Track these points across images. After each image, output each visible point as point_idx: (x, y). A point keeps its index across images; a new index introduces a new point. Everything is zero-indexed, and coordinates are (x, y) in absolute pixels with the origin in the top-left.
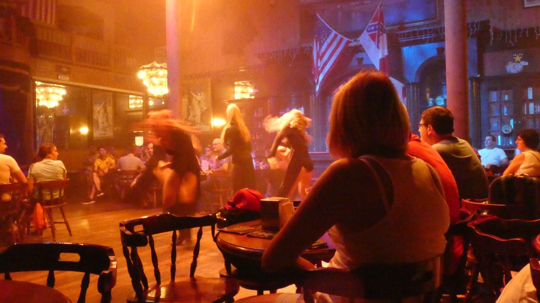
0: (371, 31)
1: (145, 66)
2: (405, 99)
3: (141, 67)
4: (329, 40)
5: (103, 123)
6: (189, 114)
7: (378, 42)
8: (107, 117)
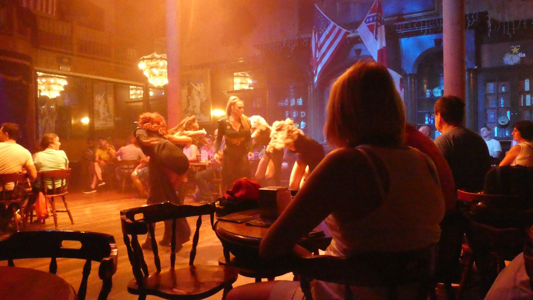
0: (369, 22)
1: (145, 57)
2: (403, 90)
3: (142, 58)
4: (327, 32)
5: (104, 114)
6: (189, 105)
7: (377, 33)
8: (108, 108)
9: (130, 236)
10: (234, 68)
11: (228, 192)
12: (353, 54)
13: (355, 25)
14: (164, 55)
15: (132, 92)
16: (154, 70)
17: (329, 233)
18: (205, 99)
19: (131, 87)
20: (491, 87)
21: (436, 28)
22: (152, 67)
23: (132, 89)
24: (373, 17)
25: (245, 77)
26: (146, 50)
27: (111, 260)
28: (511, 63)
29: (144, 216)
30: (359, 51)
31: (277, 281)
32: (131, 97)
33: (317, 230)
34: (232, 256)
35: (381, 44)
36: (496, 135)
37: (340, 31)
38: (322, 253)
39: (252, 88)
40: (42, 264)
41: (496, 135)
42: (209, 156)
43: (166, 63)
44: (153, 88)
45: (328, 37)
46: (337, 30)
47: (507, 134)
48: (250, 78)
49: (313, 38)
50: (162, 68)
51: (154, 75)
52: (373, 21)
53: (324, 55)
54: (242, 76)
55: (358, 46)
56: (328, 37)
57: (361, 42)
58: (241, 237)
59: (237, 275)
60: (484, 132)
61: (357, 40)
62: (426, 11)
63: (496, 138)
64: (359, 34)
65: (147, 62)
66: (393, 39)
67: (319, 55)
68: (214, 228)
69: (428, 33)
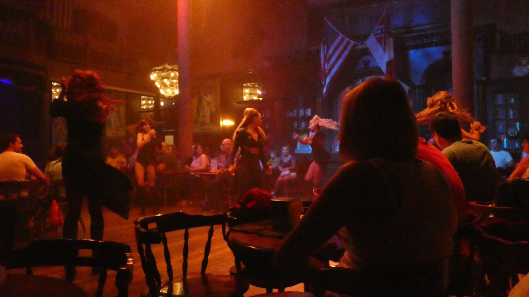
0: (378, 34)
1: (157, 68)
3: (153, 69)
4: (336, 43)
6: (199, 115)
7: (385, 45)
9: (144, 247)
10: (241, 81)
11: (239, 203)
12: (361, 65)
13: (365, 37)
14: (176, 66)
15: (143, 102)
16: (165, 81)
17: (340, 244)
18: (214, 109)
19: (143, 97)
20: (500, 99)
21: (445, 40)
22: (163, 78)
23: (144, 99)
24: (381, 29)
25: (255, 88)
26: (158, 61)
27: (128, 270)
28: (519, 74)
29: (157, 225)
30: (367, 63)
31: (289, 292)
32: (142, 107)
33: (330, 242)
34: (243, 266)
35: (389, 56)
36: (505, 146)
37: (348, 43)
38: (333, 264)
39: (261, 99)
40: (57, 272)
41: (505, 146)
42: (218, 166)
43: (177, 74)
44: (164, 97)
45: (336, 48)
46: (345, 42)
47: (517, 146)
48: (259, 89)
49: (322, 50)
50: (173, 79)
51: (165, 86)
52: (381, 33)
53: (333, 66)
54: (252, 87)
55: (367, 58)
56: (336, 48)
57: (370, 54)
58: (253, 248)
59: (248, 285)
60: (494, 144)
61: (366, 52)
62: (432, 24)
63: (505, 150)
64: (368, 46)
65: (158, 73)
66: (401, 52)
67: (327, 67)
68: (226, 238)
69: (436, 44)
